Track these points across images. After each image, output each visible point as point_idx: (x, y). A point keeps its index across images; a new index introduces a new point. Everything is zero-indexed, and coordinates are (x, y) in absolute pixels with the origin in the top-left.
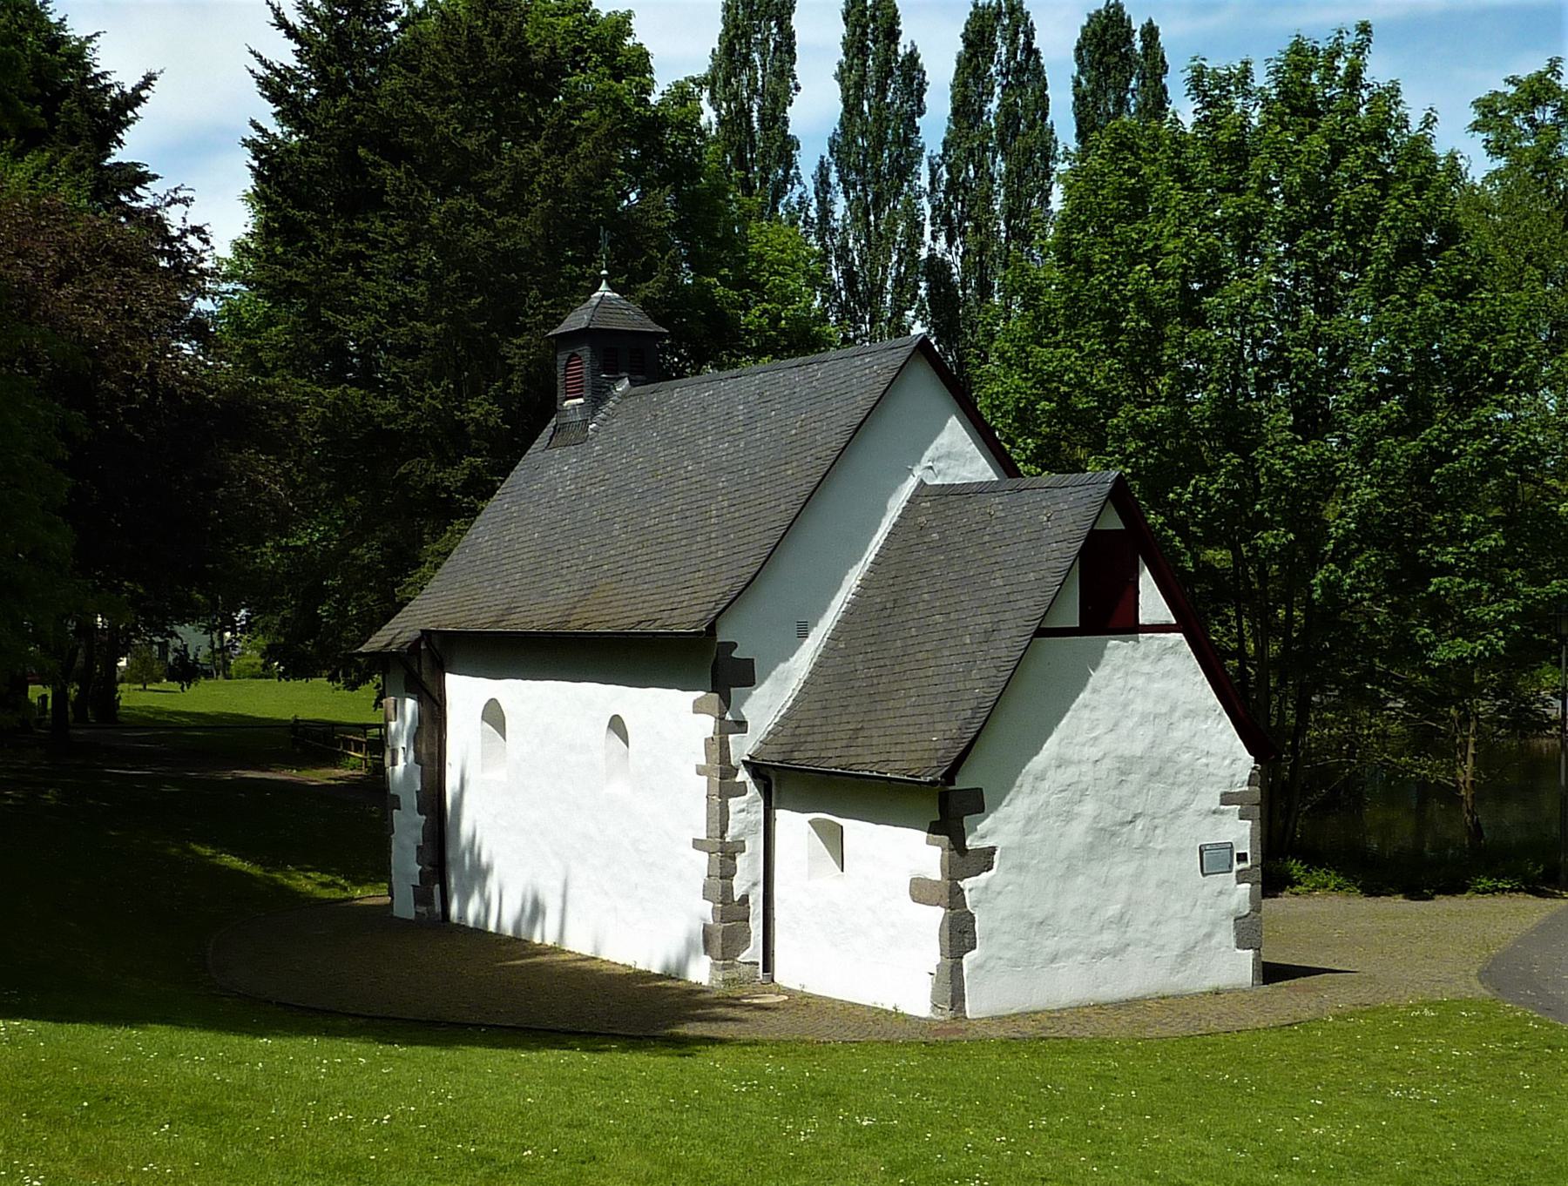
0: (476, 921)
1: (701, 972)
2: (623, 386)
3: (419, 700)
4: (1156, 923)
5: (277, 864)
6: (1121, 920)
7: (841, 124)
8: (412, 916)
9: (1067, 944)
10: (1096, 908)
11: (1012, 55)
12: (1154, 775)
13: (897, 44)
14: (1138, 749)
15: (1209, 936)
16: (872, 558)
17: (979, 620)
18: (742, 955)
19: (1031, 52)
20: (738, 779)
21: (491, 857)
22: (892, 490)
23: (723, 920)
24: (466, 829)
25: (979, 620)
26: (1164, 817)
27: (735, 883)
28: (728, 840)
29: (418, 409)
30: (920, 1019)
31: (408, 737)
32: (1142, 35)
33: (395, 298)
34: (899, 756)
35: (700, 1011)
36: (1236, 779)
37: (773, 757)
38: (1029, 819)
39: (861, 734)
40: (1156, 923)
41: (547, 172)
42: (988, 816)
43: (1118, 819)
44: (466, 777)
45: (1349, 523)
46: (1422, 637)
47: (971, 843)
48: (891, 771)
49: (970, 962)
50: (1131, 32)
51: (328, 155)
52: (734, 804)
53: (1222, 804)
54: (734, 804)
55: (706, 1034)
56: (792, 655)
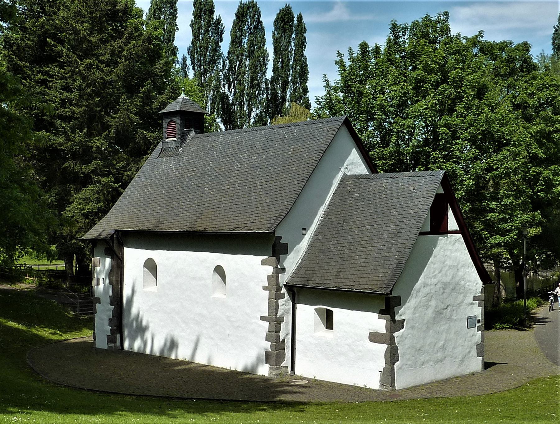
0: (139, 349)
1: (264, 371)
2: (192, 134)
3: (112, 258)
4: (454, 348)
5: (30, 325)
6: (443, 348)
7: (192, 43)
8: (106, 348)
9: (427, 358)
10: (436, 343)
11: (252, 23)
12: (453, 289)
13: (213, 15)
14: (448, 279)
15: (469, 352)
16: (328, 203)
17: (389, 228)
18: (283, 363)
19: (259, 22)
20: (282, 292)
21: (148, 321)
22: (334, 177)
23: (276, 349)
24: (134, 311)
25: (389, 228)
26: (456, 306)
27: (280, 334)
28: (278, 317)
29: (74, 141)
30: (376, 390)
31: (106, 273)
32: (298, 18)
33: (63, 97)
34: (365, 283)
35: (279, 389)
36: (478, 291)
37: (298, 282)
38: (415, 308)
39: (341, 274)
40: (454, 348)
41: (127, 51)
42: (402, 307)
43: (442, 307)
44: (136, 288)
45: (462, 193)
46: (485, 235)
47: (397, 318)
48: (363, 289)
49: (397, 367)
50: (293, 17)
51: (33, 41)
52: (281, 302)
53: (473, 301)
54: (281, 302)
55: (296, 400)
56: (301, 242)
